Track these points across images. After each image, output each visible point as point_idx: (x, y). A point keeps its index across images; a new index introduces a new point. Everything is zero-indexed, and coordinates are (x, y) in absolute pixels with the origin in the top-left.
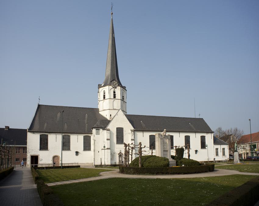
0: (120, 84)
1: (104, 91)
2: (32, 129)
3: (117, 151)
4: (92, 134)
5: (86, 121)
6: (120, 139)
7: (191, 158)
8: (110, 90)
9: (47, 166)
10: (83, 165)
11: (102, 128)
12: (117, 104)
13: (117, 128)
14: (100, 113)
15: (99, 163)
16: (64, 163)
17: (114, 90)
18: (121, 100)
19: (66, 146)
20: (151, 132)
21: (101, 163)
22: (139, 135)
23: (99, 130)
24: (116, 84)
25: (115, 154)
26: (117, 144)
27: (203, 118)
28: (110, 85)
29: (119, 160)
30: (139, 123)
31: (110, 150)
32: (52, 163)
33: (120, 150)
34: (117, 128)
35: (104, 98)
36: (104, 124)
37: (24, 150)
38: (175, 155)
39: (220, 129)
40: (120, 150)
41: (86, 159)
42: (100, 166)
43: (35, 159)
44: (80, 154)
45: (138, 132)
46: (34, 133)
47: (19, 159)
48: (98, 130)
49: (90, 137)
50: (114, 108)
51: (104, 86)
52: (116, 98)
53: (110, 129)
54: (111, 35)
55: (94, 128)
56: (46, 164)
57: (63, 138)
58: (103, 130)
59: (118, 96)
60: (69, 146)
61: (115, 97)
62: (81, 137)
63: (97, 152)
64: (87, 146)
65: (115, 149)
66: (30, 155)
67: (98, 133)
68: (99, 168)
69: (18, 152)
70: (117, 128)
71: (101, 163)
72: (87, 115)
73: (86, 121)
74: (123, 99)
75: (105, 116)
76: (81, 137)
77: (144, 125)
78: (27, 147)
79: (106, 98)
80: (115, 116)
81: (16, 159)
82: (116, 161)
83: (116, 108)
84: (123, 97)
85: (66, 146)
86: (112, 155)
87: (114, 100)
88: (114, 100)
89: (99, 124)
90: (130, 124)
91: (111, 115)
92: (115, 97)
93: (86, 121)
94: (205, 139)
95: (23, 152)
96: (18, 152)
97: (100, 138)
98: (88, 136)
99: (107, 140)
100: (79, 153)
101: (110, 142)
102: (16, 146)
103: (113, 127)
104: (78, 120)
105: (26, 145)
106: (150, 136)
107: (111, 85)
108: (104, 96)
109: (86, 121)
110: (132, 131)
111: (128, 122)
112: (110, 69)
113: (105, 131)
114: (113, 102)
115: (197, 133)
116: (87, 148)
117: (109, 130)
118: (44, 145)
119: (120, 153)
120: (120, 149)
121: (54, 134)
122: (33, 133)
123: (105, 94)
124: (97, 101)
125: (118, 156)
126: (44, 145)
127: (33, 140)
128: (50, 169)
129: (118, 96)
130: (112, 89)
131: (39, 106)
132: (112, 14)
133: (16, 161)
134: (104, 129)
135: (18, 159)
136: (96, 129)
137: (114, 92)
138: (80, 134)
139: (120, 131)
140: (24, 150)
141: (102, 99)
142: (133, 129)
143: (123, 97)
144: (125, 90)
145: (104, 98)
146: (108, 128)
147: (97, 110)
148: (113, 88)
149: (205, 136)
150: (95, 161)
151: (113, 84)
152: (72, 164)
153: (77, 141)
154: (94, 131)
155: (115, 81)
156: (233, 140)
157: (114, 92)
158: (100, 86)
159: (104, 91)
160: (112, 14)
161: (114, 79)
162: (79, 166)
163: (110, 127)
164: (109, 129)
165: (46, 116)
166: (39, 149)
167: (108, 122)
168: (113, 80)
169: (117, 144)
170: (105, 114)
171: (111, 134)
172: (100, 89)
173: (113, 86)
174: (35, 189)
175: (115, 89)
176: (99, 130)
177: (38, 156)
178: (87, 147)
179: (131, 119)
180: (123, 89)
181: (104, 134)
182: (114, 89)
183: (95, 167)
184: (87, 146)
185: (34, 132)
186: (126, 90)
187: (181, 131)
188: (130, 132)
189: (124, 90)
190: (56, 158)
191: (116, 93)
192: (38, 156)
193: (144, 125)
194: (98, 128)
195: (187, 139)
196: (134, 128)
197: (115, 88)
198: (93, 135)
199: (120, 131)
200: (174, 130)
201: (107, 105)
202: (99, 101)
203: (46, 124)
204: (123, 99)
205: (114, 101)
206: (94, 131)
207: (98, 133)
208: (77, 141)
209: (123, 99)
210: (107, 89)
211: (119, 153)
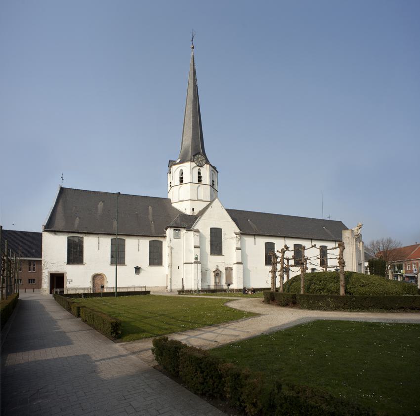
0: (207, 162)
1: (182, 170)
2: (50, 227)
3: (212, 267)
4: (165, 237)
5: (149, 218)
6: (217, 247)
8: (192, 169)
9: (86, 292)
10: (156, 289)
11: (184, 228)
12: (205, 192)
13: (211, 229)
14: (173, 205)
17: (199, 169)
18: (211, 186)
19: (118, 257)
20: (267, 237)
21: (183, 286)
22: (249, 240)
23: (180, 230)
24: (203, 160)
25: (208, 272)
26: (211, 254)
28: (192, 162)
29: (216, 282)
30: (249, 223)
31: (242, 265)
32: (92, 287)
33: (217, 266)
34: (211, 229)
35: (181, 181)
37: (30, 265)
39: (390, 241)
40: (217, 266)
41: (155, 280)
42: (195, 291)
43: (58, 280)
44: (143, 271)
45: (246, 236)
46: (56, 234)
47: (34, 280)
48: (177, 230)
49: (162, 242)
50: (199, 198)
51: (181, 162)
52: (202, 182)
53: (200, 230)
54: (191, 81)
55: (171, 227)
56: (84, 289)
57: (152, 244)
58: (187, 230)
59: (206, 179)
62: (145, 243)
63: (175, 267)
64: (156, 258)
65: (209, 263)
66: (48, 272)
67: (177, 236)
68: (185, 294)
70: (211, 229)
71: (183, 286)
72: (150, 207)
73: (150, 217)
74: (213, 184)
75: (184, 211)
76: (145, 243)
77: (255, 227)
78: (41, 261)
79: (184, 182)
81: (29, 280)
82: (210, 283)
83: (202, 199)
84: (213, 181)
85: (118, 257)
86: (204, 273)
87: (199, 186)
88: (199, 186)
89: (179, 222)
90: (233, 223)
91: (193, 209)
93: (150, 217)
94: (42, 237)
95: (28, 269)
97: (180, 247)
98: (158, 241)
100: (140, 270)
101: (242, 252)
102: (25, 259)
103: (204, 226)
104: (137, 214)
105: (41, 257)
106: (294, 245)
107: (194, 161)
109: (149, 218)
110: (236, 234)
111: (230, 219)
112: (191, 136)
113: (191, 234)
114: (179, 189)
115: (288, 239)
116: (156, 261)
117: (198, 231)
118: (75, 255)
119: (217, 269)
120: (217, 264)
121: (95, 236)
122: (54, 233)
123: (182, 173)
125: (213, 275)
126: (75, 255)
127: (54, 248)
128: (94, 298)
129: (206, 179)
130: (194, 167)
131: (62, 190)
132: (193, 48)
133: (29, 283)
134: (189, 229)
135: (32, 280)
136: (174, 230)
137: (199, 173)
138: (144, 238)
139: (216, 235)
140: (30, 265)
141: (179, 183)
142: (238, 230)
143: (213, 181)
144: (216, 171)
145: (181, 181)
147: (168, 201)
148: (198, 166)
149: (273, 244)
150: (173, 283)
151: (198, 159)
152: (135, 288)
153: (97, 248)
154: (170, 232)
155: (200, 156)
156: (389, 255)
157: (199, 173)
158: (172, 163)
159: (182, 170)
160: (193, 48)
161: (197, 152)
162: (149, 292)
163: (198, 225)
165: (76, 207)
166: (66, 261)
168: (199, 153)
169: (211, 254)
170: (185, 208)
171: (201, 237)
172: (174, 167)
173: (198, 164)
174: (415, 325)
175: (201, 168)
176: (180, 230)
177: (63, 274)
178: (155, 259)
179: (236, 216)
180: (214, 170)
181: (188, 238)
182: (198, 168)
183: (178, 293)
184: (156, 258)
185: (55, 232)
186: (218, 172)
187: (313, 237)
188: (234, 235)
189: (215, 172)
190: (98, 278)
191: (202, 175)
192: (63, 274)
193: (254, 226)
194: (177, 228)
196: (240, 229)
197: (202, 166)
198: (168, 239)
199: (216, 235)
200: (266, 233)
201: (183, 192)
202: (169, 188)
203: (77, 220)
204: (213, 184)
205: (200, 188)
206: (170, 232)
207: (177, 237)
208: (137, 249)
209: (212, 185)
210: (186, 167)
211: (214, 270)
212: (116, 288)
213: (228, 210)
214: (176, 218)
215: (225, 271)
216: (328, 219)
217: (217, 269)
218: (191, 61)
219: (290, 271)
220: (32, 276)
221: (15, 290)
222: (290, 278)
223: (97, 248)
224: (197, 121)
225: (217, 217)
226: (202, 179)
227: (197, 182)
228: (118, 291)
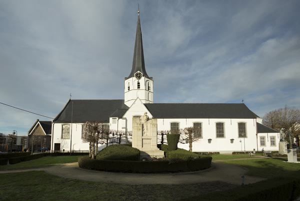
14: (125, 103)
35: (129, 89)
43: (58, 146)
52: (140, 88)
74: (149, 89)
108: (129, 87)
126: (65, 133)
127: (57, 128)
137: (139, 83)
141: (128, 90)
146: (124, 116)
157: (139, 83)
206: (111, 119)
213: (146, 105)
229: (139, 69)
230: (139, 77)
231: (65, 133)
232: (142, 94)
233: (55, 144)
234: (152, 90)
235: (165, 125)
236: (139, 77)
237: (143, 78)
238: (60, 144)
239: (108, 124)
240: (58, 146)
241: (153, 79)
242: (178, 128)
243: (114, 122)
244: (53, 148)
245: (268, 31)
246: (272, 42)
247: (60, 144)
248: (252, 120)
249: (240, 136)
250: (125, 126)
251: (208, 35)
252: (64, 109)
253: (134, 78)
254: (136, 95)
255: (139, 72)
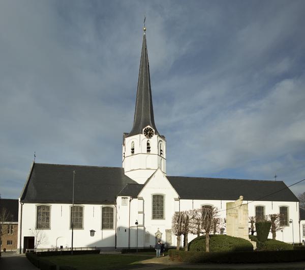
7: (277, 239)
14: (126, 174)
15: (126, 246)
16: (76, 247)
17: (148, 141)
27: (282, 182)
30: (186, 187)
31: (142, 201)
35: (133, 152)
36: (134, 190)
38: (268, 238)
43: (29, 241)
52: (151, 152)
59: (154, 149)
60: (162, 212)
61: (149, 151)
69: (10, 231)
74: (161, 154)
79: (135, 153)
80: (149, 179)
81: (8, 241)
92: (149, 151)
96: (10, 231)
99: (139, 213)
103: (146, 194)
108: (133, 149)
109: (104, 185)
119: (158, 231)
124: (120, 156)
126: (43, 221)
127: (28, 212)
129: (154, 149)
131: (34, 164)
137: (148, 144)
139: (158, 201)
141: (131, 154)
143: (161, 151)
145: (133, 152)
146: (140, 195)
157: (148, 144)
164: (142, 197)
167: (141, 187)
170: (138, 177)
179: (175, 182)
191: (151, 146)
194: (125, 194)
195: (284, 210)
199: (158, 201)
202: (123, 158)
206: (119, 199)
212: (72, 248)
213: (168, 178)
214: (125, 184)
215: (165, 232)
216: (274, 180)
217: (158, 231)
218: (142, 39)
219: (104, 238)
220: (10, 239)
221: (159, 252)
222: (189, 242)
223: (60, 212)
224: (148, 95)
225: (162, 186)
226: (151, 149)
227: (146, 152)
228: (74, 250)
229: (145, 124)
230: (149, 134)
231: (43, 221)
232: (153, 160)
233: (25, 238)
234: (164, 155)
235: (192, 206)
236: (149, 134)
237: (155, 137)
238: (34, 237)
239: (113, 206)
240: (29, 241)
241: (166, 139)
242: (263, 213)
243: (124, 204)
244: (20, 244)
245: (284, 65)
246: (288, 84)
247: (34, 237)
248: (294, 203)
249: (73, 226)
250: (142, 211)
251: (200, 60)
252: (29, 180)
253: (143, 136)
254: (142, 160)
255: (149, 127)
